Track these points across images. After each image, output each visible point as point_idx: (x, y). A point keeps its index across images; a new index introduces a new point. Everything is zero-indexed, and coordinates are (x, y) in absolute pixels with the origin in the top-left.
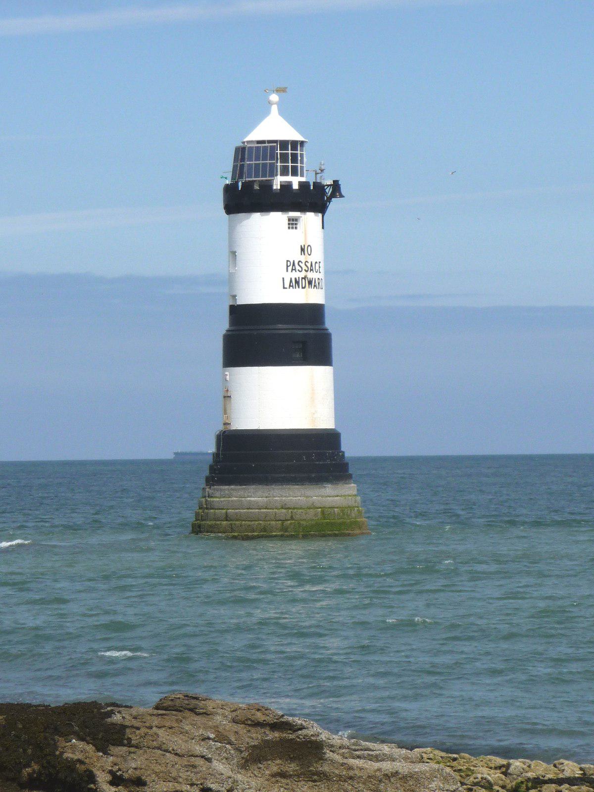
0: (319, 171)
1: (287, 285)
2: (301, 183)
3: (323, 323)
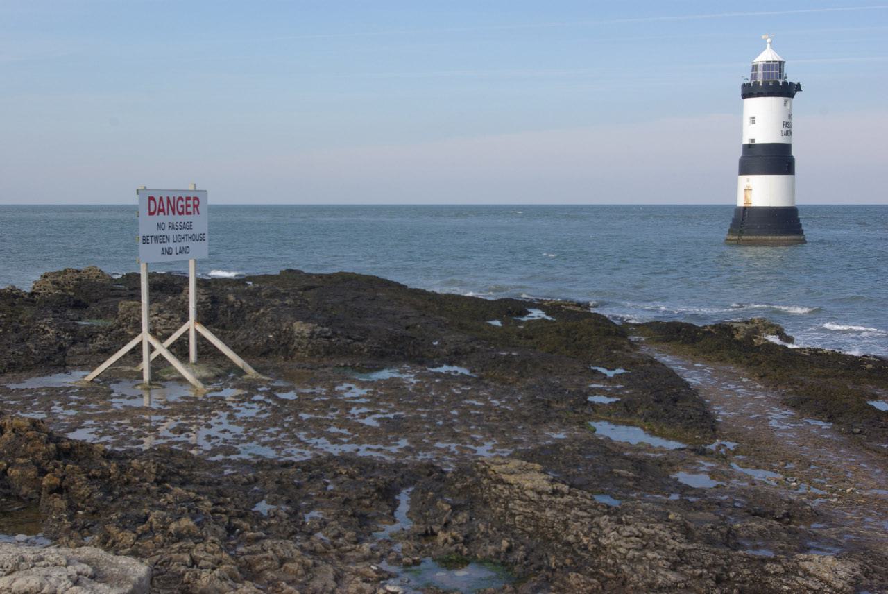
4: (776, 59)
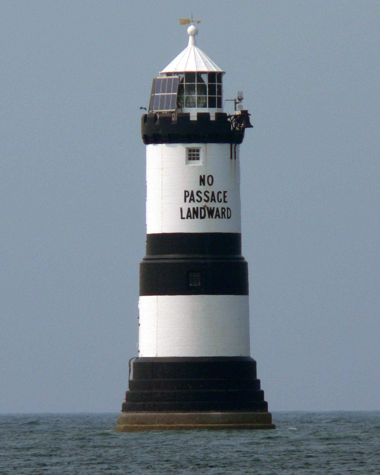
0: (237, 101)
1: (185, 215)
2: (199, 115)
3: (241, 254)
4: (203, 68)
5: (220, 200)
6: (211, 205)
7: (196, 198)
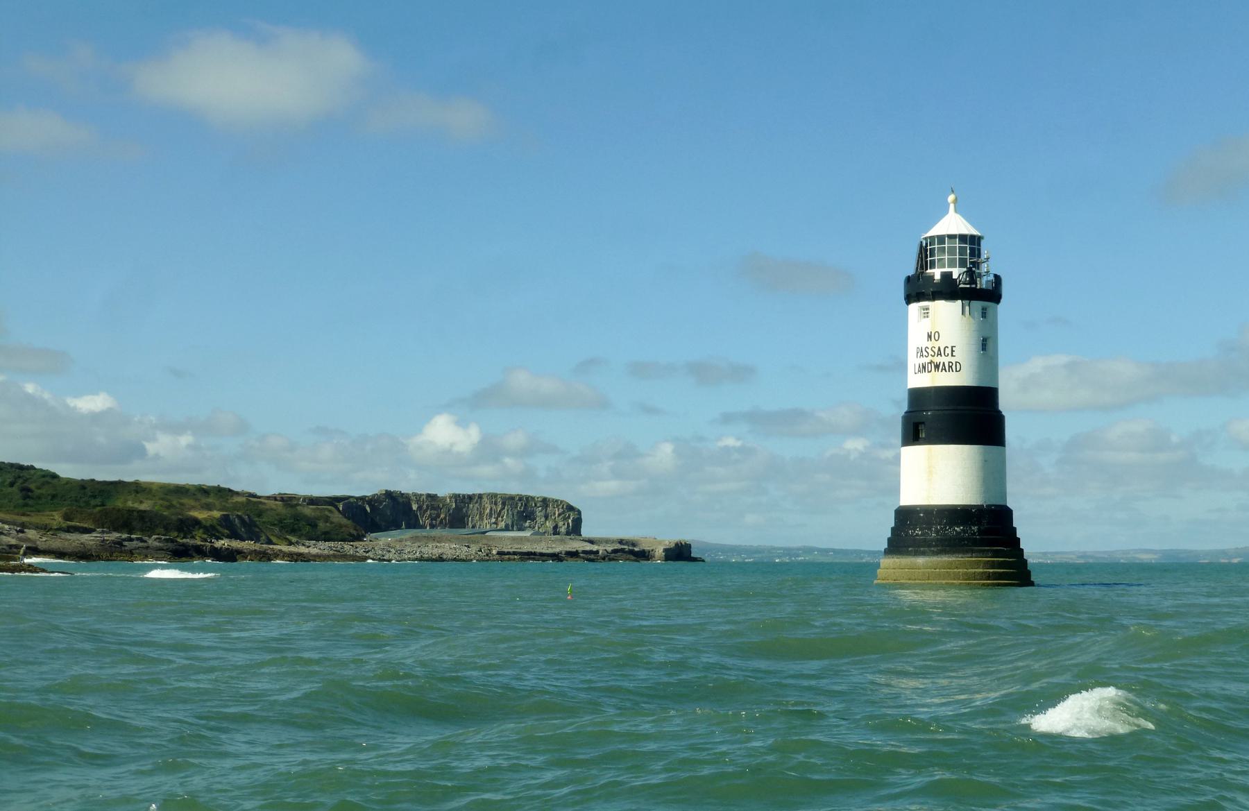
1: (917, 371)
5: (946, 354)
6: (937, 359)
7: (925, 353)
